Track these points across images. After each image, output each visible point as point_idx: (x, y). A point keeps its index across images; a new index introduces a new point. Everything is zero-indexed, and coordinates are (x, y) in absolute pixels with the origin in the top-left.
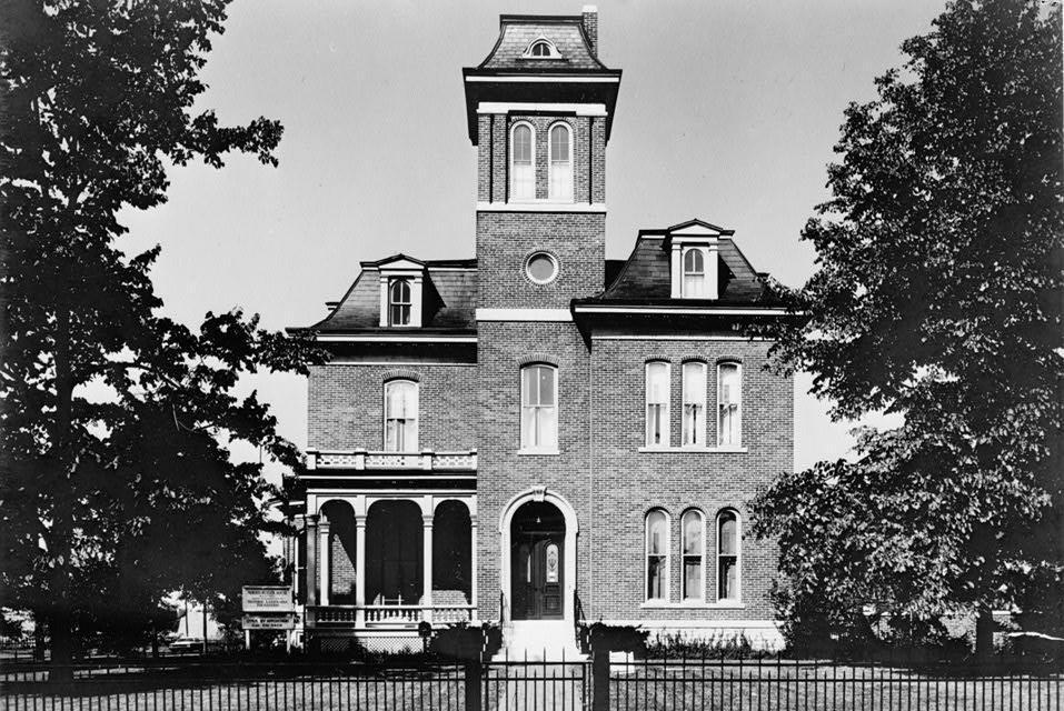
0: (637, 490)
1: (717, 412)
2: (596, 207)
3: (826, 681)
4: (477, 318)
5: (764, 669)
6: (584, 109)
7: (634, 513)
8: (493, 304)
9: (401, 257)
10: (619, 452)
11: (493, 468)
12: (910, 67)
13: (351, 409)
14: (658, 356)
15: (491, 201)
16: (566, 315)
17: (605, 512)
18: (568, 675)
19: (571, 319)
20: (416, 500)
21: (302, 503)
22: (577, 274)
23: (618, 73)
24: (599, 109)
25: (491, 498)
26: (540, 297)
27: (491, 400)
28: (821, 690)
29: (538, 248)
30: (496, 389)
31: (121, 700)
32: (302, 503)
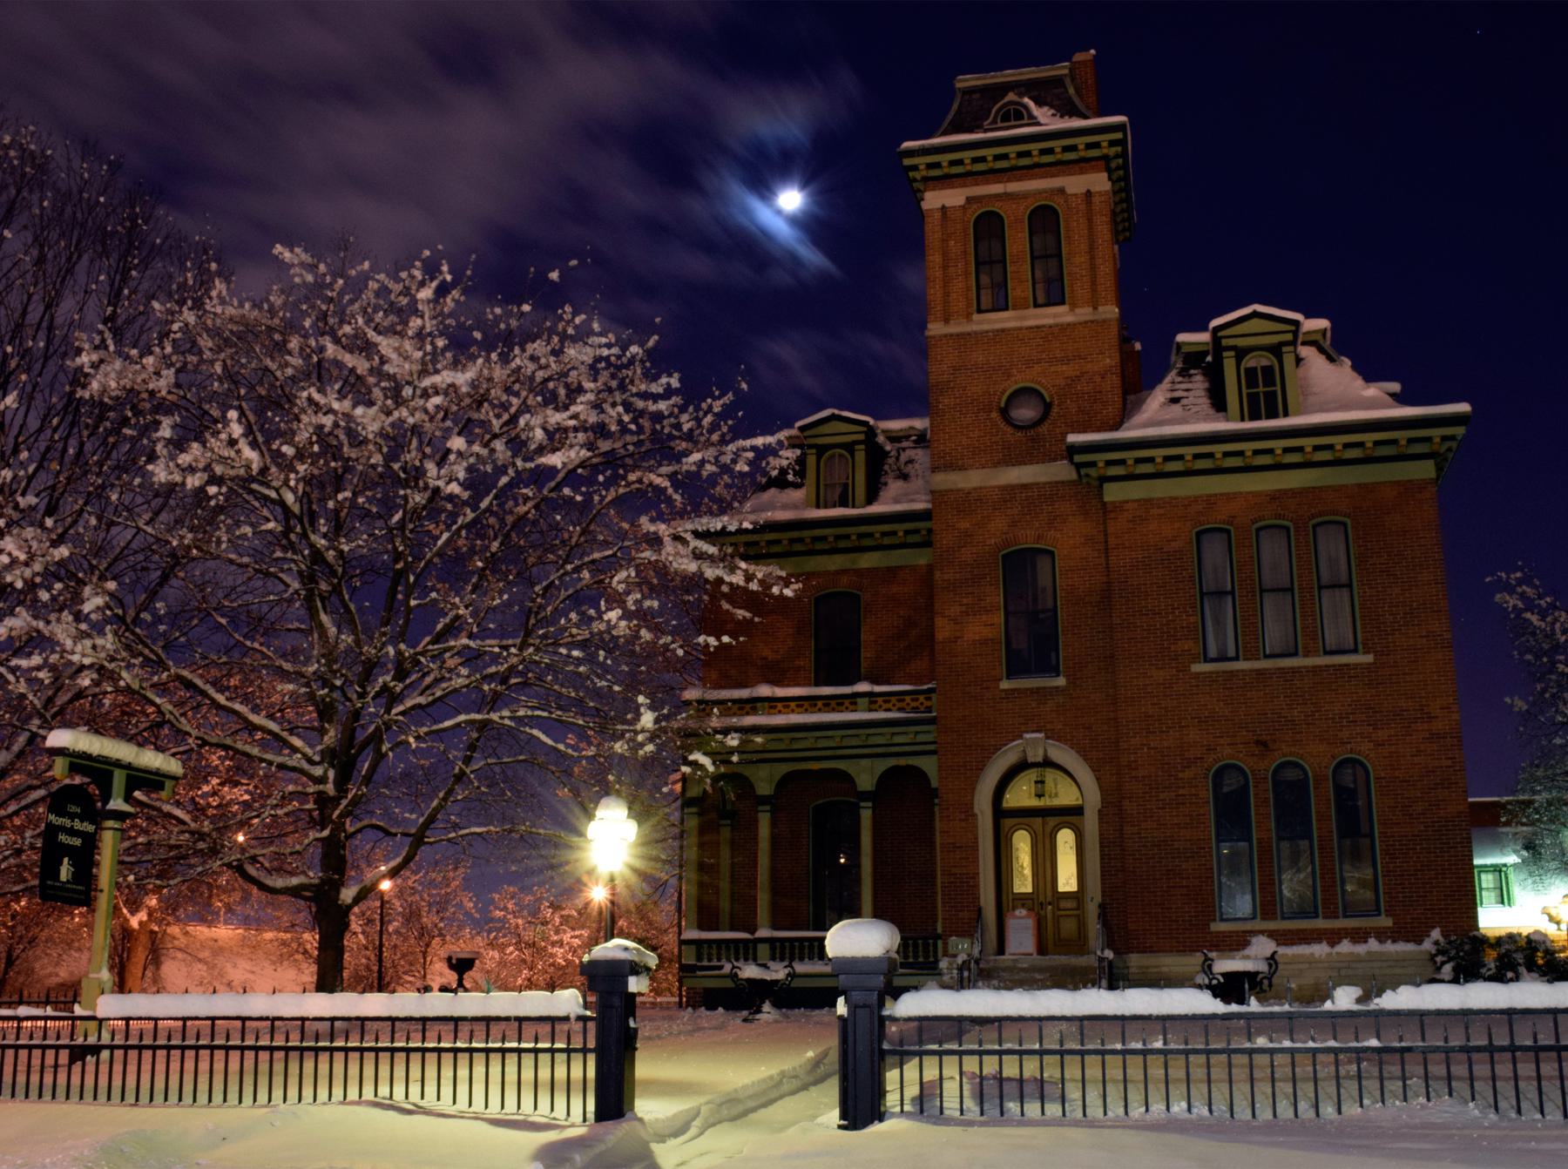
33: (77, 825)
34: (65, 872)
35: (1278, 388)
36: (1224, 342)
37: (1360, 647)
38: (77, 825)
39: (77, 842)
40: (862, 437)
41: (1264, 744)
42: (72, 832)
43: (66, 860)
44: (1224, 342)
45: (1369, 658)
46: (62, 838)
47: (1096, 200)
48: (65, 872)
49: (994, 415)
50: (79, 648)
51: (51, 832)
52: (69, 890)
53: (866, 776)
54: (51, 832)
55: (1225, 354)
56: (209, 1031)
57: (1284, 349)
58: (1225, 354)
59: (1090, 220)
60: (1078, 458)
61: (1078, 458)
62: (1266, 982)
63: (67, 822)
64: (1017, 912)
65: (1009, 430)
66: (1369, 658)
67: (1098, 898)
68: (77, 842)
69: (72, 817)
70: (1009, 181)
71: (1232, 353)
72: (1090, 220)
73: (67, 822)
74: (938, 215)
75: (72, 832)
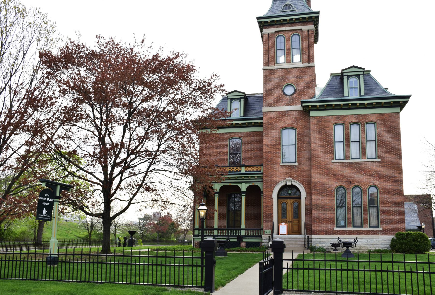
0: (331, 179)
1: (363, 142)
2: (311, 64)
3: (342, 270)
4: (263, 111)
5: (339, 264)
6: (305, 28)
7: (330, 189)
8: (269, 105)
9: (235, 91)
10: (323, 163)
11: (270, 171)
12: (69, 41)
13: (216, 150)
14: (339, 122)
15: (309, 63)
16: (299, 107)
17: (317, 188)
18: (306, 267)
19: (302, 109)
20: (239, 185)
21: (59, 187)
22: (304, 91)
23: (318, 12)
24: (311, 27)
25: (269, 183)
26: (289, 100)
27: (269, 144)
28: (385, 277)
29: (287, 82)
30: (271, 139)
31: (120, 267)
32: (59, 187)
33: (48, 199)
34: (44, 212)
35: (288, 10)
36: (344, 74)
37: (377, 157)
38: (48, 199)
39: (48, 204)
40: (243, 97)
41: (350, 182)
42: (46, 201)
43: (45, 209)
44: (344, 74)
45: (380, 160)
46: (44, 203)
47: (310, 33)
48: (44, 212)
49: (281, 92)
50: (35, 149)
51: (40, 201)
52: (45, 217)
53: (244, 187)
54: (40, 201)
55: (344, 77)
56: (122, 259)
57: (361, 76)
58: (344, 77)
59: (308, 39)
60: (304, 105)
61: (304, 105)
62: (354, 245)
63: (45, 199)
64: (282, 224)
65: (285, 96)
66: (380, 160)
67: (305, 221)
68: (48, 204)
69: (47, 197)
70: (286, 27)
71: (346, 77)
72: (308, 39)
73: (45, 199)
74: (267, 36)
75: (46, 201)
